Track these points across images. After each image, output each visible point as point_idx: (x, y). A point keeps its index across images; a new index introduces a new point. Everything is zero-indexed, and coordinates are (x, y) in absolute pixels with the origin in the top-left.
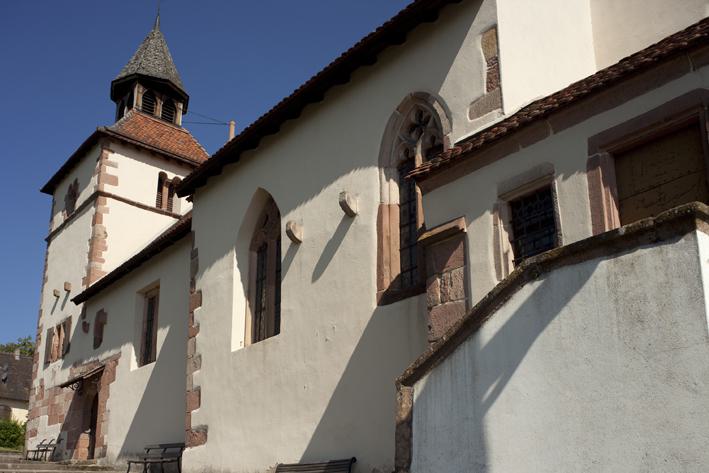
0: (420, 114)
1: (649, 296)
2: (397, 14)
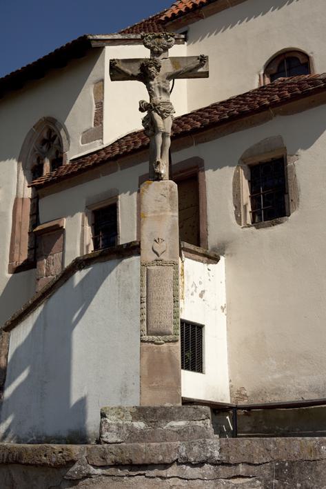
0: (50, 132)
1: (134, 285)
2: (47, 54)
